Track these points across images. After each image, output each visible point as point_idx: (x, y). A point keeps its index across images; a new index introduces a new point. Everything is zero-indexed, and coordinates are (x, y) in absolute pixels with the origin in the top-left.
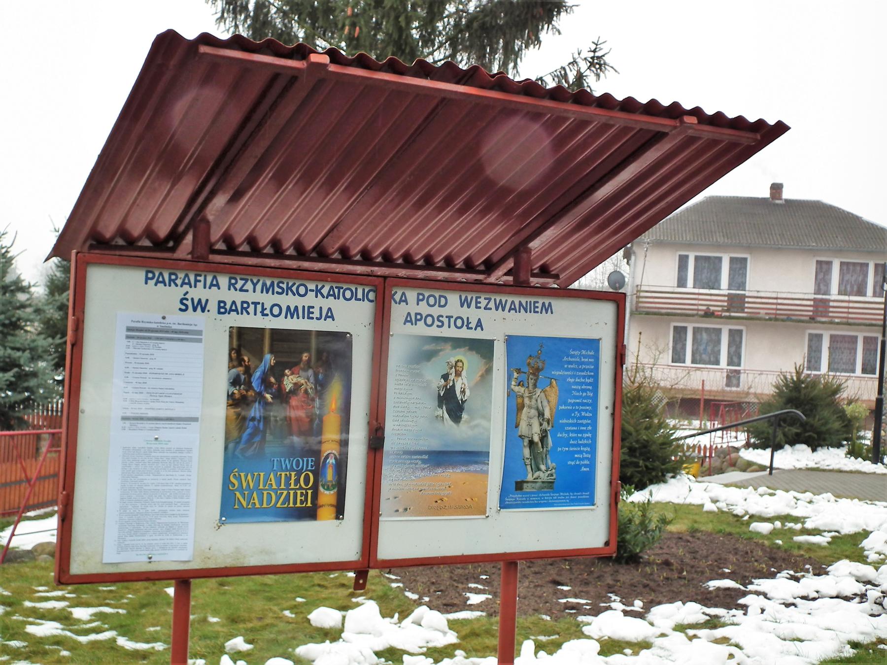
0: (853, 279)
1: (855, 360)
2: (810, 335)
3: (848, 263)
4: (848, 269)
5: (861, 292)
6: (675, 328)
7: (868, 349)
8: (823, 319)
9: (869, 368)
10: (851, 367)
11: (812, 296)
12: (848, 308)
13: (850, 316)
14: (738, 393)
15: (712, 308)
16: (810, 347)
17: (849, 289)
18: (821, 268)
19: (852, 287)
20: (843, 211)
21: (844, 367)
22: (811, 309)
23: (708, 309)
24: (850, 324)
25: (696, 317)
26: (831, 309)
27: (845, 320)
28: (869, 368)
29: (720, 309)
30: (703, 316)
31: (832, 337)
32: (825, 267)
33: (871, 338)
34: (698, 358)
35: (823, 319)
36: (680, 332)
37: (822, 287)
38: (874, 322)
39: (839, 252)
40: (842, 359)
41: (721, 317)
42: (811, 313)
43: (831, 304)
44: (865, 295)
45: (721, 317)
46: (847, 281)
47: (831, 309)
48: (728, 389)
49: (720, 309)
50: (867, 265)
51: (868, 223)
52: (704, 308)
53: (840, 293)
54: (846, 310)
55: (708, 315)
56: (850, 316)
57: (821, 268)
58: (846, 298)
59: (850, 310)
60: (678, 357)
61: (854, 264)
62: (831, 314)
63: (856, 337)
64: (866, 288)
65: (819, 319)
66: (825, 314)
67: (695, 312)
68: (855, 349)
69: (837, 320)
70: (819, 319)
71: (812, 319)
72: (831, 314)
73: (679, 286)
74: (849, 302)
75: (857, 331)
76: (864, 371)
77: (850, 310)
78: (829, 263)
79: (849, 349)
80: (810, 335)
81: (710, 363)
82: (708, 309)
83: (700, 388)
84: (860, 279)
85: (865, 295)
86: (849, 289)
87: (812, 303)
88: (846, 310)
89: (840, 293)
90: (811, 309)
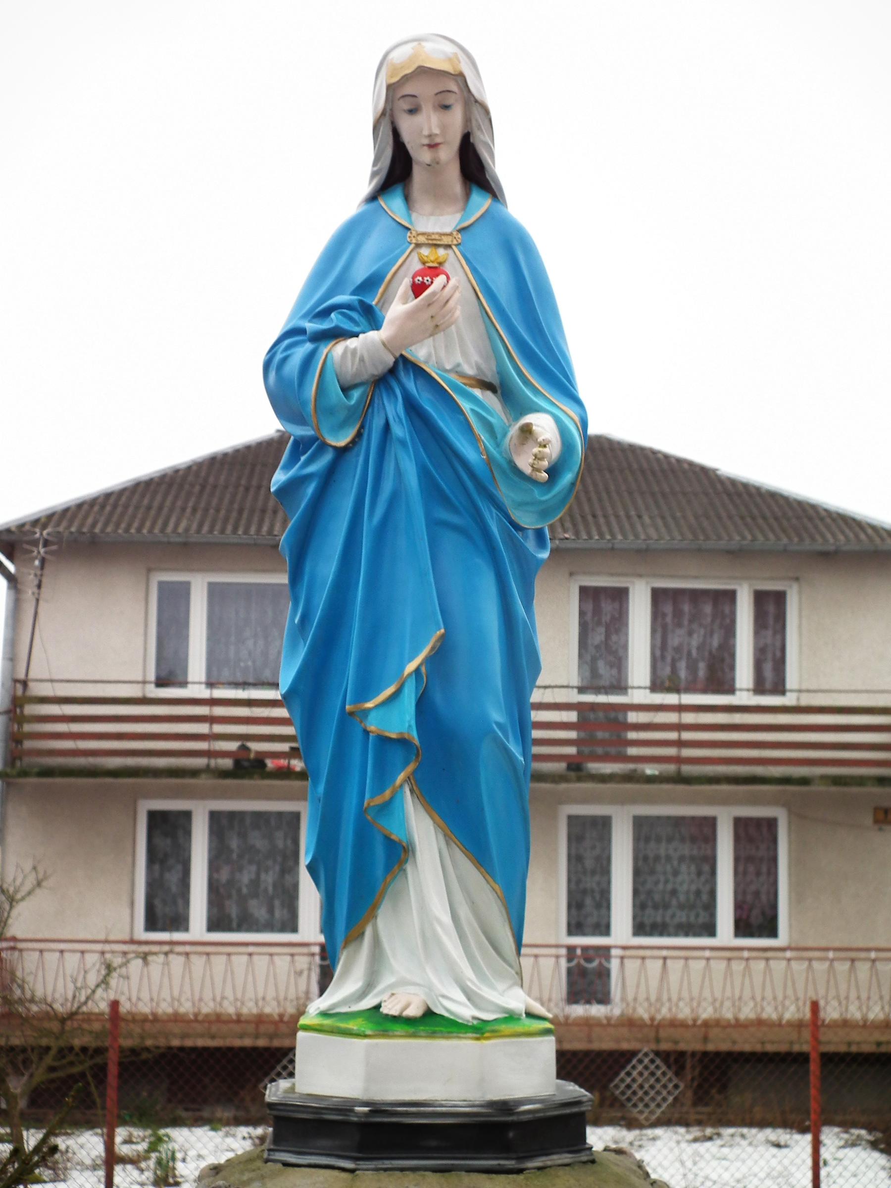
0: (695, 642)
1: (713, 894)
2: (572, 820)
3: (676, 595)
4: (678, 614)
5: (720, 679)
6: (153, 816)
7: (750, 859)
8: (608, 768)
9: (756, 918)
10: (703, 918)
11: (575, 697)
12: (680, 727)
13: (687, 752)
14: (608, 1023)
15: (256, 747)
16: (575, 859)
17: (683, 674)
18: (597, 611)
19: (692, 669)
20: (667, 457)
21: (682, 917)
22: (572, 735)
23: (244, 748)
24: (680, 779)
25: (203, 781)
26: (632, 735)
27: (671, 768)
28: (756, 918)
29: (285, 747)
30: (224, 774)
31: (640, 824)
32: (608, 608)
33: (758, 822)
34: (233, 910)
35: (608, 768)
36: (168, 830)
37: (602, 667)
38: (759, 770)
39: (644, 557)
40: (674, 892)
41: (286, 773)
42: (572, 750)
43: (633, 717)
44: (731, 690)
45: (286, 773)
46: (678, 650)
47: (632, 735)
48: (578, 1010)
49: (285, 747)
50: (731, 596)
51: (733, 482)
52: (233, 746)
53: (656, 686)
54: (672, 736)
55: (248, 767)
56: (687, 752)
57: (597, 611)
58: (671, 699)
59: (687, 736)
60: (165, 912)
61: (696, 595)
62: (632, 751)
63: (711, 823)
64: (732, 668)
65: (595, 767)
66: (616, 748)
67: (201, 762)
68: (711, 861)
69: (650, 770)
70: (595, 767)
71: (576, 768)
72: (632, 751)
73: (161, 683)
74: (681, 708)
75: (712, 801)
76: (743, 928)
77: (687, 736)
78: (620, 595)
79: (693, 859)
80: (572, 820)
81: (269, 927)
82: (244, 748)
83: (808, 1015)
84: (715, 642)
85: (731, 690)
86: (683, 674)
87: (572, 716)
88: (672, 736)
89: (656, 686)
90: (572, 735)
